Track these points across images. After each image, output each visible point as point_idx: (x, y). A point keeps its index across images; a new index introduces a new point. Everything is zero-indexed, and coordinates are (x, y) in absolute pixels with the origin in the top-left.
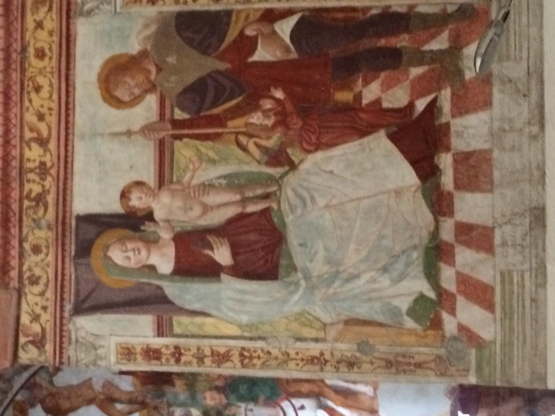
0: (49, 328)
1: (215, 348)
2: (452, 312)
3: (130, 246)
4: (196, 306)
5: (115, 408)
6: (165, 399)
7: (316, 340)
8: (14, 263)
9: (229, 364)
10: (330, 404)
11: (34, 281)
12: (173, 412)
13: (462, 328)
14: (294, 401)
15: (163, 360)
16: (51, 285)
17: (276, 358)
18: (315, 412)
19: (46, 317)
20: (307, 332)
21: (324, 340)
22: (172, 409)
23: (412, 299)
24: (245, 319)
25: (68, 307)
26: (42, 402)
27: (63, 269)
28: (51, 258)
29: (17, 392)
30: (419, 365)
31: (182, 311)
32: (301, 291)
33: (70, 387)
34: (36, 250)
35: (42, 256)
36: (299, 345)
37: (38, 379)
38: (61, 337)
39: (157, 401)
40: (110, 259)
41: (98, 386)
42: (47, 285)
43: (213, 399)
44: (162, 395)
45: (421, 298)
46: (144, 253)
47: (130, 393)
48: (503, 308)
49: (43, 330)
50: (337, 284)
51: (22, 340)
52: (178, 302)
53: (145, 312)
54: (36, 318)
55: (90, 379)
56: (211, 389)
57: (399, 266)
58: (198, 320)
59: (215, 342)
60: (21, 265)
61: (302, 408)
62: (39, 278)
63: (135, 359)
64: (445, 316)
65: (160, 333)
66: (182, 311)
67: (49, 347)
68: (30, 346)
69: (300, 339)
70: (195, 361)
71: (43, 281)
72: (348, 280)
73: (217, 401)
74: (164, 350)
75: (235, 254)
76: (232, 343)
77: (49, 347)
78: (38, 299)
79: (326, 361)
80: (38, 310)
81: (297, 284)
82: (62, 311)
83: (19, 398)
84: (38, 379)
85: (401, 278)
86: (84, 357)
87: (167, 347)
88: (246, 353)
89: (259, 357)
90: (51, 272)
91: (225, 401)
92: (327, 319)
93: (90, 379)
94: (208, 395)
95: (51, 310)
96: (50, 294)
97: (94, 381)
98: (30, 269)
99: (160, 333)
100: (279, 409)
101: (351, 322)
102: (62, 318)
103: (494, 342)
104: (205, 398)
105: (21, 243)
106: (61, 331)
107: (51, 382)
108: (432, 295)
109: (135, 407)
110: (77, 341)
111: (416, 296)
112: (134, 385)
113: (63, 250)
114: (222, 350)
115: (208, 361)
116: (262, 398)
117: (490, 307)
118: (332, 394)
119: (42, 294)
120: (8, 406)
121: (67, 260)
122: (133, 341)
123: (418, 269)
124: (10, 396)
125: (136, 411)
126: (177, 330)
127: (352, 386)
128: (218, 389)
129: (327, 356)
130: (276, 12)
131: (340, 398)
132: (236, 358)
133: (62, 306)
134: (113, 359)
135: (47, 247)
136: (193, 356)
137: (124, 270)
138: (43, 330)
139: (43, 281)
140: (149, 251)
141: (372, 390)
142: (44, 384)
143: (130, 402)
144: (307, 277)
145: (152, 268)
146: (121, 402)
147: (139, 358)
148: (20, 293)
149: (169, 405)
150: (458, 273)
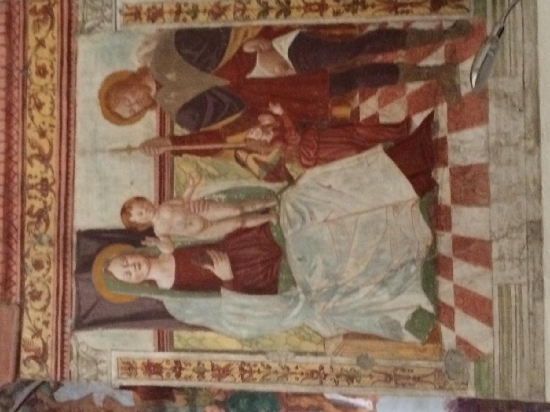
107: (52, 398)
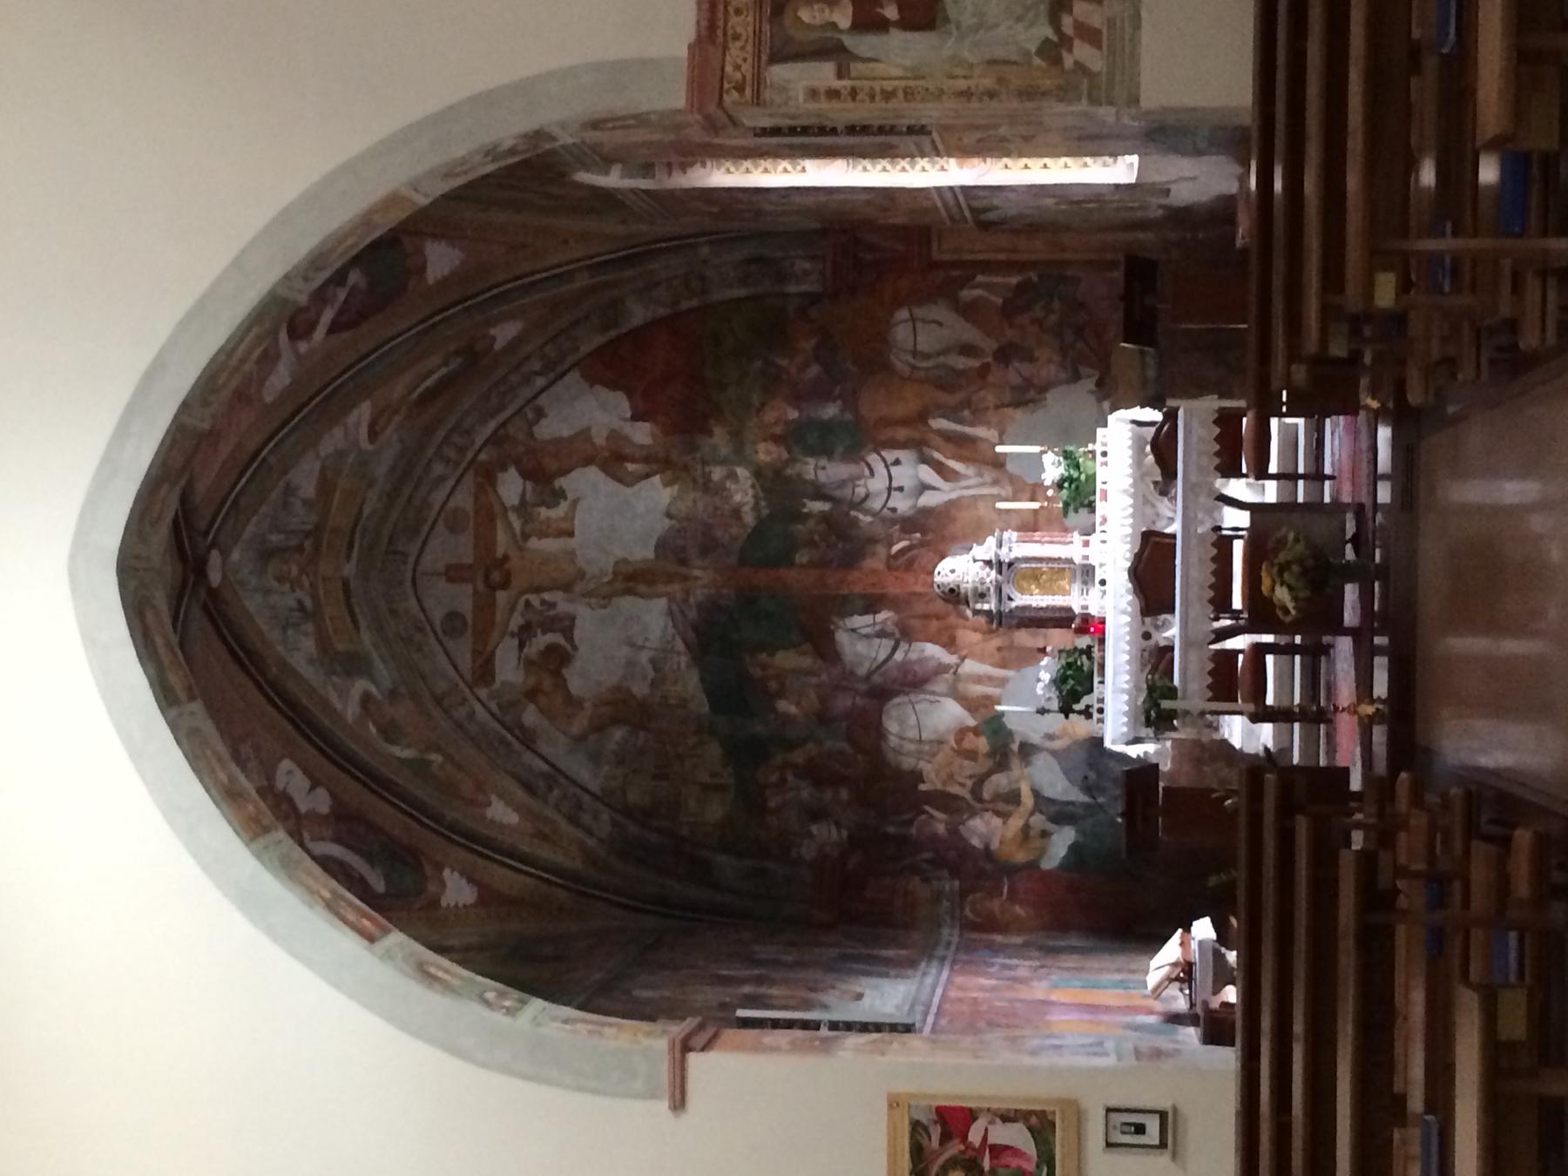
0: (749, 77)
1: (885, 88)
2: (1070, 50)
3: (816, 7)
4: (869, 55)
5: (626, 468)
6: (698, 455)
7: (965, 77)
8: (721, 23)
9: (894, 100)
10: (937, 455)
11: (736, 37)
12: (710, 472)
13: (1077, 63)
14: (884, 453)
15: (842, 98)
16: (751, 41)
17: (932, 93)
18: (916, 468)
19: (747, 68)
20: (958, 71)
21: (971, 77)
22: (707, 469)
23: (1039, 42)
24: (908, 63)
25: (764, 57)
26: (517, 463)
27: (760, 27)
28: (750, 19)
29: (480, 450)
30: (1044, 94)
31: (857, 58)
32: (953, 39)
33: (558, 441)
34: (738, 12)
35: (743, 17)
36: (951, 81)
37: (511, 430)
38: (759, 83)
39: (687, 459)
40: (800, 18)
41: (600, 439)
42: (747, 41)
43: (768, 453)
44: (692, 448)
45: (1047, 41)
46: (827, 11)
47: (649, 446)
48: (1109, 47)
49: (744, 77)
50: (981, 32)
51: (726, 86)
52: (855, 51)
53: (829, 60)
54: (738, 67)
55: (589, 429)
56: (765, 440)
57: (1031, 15)
58: (871, 65)
59: (885, 82)
60: (726, 23)
61: (897, 462)
62: (741, 34)
63: (820, 98)
64: (1065, 54)
65: (840, 76)
66: (857, 58)
67: (748, 91)
68: (733, 91)
69: (952, 77)
70: (867, 98)
71: (744, 37)
72: (990, 28)
73: (775, 456)
74: (842, 91)
75: (901, 10)
76: (897, 83)
77: (748, 91)
78: (738, 52)
79: (972, 94)
80: (739, 61)
81: (950, 34)
82: (759, 62)
83: (483, 457)
84: (511, 430)
85: (1032, 25)
86: (778, 99)
87: (845, 88)
88: (909, 90)
89: (919, 93)
90: (750, 29)
91: (785, 455)
92: (971, 59)
93: (589, 429)
94: (762, 447)
95: (750, 60)
96: (749, 48)
97: (594, 431)
98: (733, 28)
99: (840, 76)
100: (863, 464)
101: (993, 62)
102: (759, 67)
103: (1100, 73)
104: (757, 452)
105: (725, 7)
106: (758, 77)
107: (531, 435)
108: (1055, 38)
109: (655, 467)
110: (771, 86)
111: (1043, 39)
112: (652, 435)
113: (761, 12)
114: (890, 89)
115: (878, 98)
116: (840, 450)
117: (1099, 47)
118: (938, 441)
119: (742, 48)
120: (466, 470)
121: (764, 20)
122: (816, 84)
123: (1043, 19)
124: (470, 455)
125: (655, 474)
126: (853, 74)
127: (968, 430)
128: (777, 439)
129: (973, 90)
130: (653, 117)
131: (951, 447)
132: (901, 94)
133: (759, 58)
134: (801, 98)
135: (747, 10)
136: (866, 94)
137: (809, 27)
138: (744, 77)
139: (744, 37)
140: (832, 11)
141: (996, 433)
142: (521, 436)
143: (647, 460)
144: (958, 28)
145: (834, 25)
146: (633, 461)
147: (823, 98)
148: (725, 48)
149: (705, 463)
150: (1076, 21)
